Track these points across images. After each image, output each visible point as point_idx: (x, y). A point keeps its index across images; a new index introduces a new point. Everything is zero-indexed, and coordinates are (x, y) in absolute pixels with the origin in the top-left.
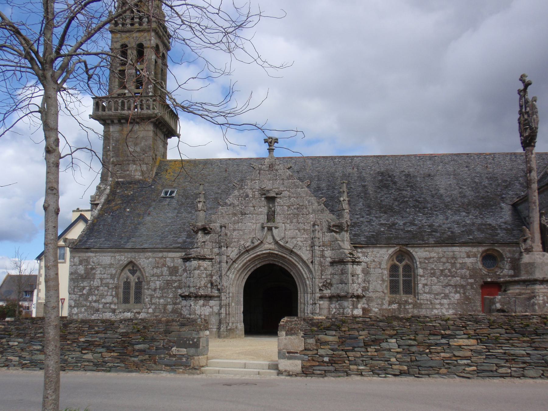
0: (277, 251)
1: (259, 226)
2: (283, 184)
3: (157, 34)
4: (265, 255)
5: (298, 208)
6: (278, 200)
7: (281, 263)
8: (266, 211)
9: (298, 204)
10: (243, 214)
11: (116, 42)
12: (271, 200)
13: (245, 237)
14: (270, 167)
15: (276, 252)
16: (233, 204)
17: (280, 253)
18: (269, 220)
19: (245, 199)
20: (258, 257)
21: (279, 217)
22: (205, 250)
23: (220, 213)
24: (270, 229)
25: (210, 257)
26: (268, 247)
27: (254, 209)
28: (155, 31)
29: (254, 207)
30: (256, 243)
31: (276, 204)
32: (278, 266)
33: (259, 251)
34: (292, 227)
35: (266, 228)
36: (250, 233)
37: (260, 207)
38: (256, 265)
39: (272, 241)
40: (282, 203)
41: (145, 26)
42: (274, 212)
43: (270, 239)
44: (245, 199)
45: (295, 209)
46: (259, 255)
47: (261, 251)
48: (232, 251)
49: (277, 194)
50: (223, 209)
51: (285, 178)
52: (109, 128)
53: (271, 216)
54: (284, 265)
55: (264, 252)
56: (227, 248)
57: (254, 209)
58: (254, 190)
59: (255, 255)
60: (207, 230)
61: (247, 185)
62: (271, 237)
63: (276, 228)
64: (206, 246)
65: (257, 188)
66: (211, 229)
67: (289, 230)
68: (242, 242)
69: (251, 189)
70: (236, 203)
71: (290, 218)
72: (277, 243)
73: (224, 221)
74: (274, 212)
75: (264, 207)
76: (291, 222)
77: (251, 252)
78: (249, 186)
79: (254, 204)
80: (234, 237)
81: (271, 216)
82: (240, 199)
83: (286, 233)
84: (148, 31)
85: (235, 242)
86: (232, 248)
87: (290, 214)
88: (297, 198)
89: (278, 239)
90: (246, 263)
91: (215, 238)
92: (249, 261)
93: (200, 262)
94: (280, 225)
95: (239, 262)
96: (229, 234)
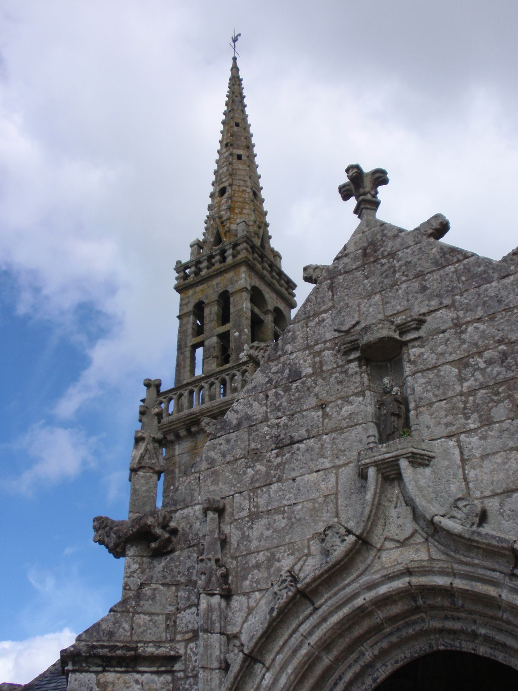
0: (442, 573)
1: (348, 473)
2: (424, 289)
3: (251, 268)
4: (395, 609)
5: (504, 356)
6: (414, 351)
7: (487, 639)
8: (371, 410)
9: (501, 342)
10: (284, 444)
11: (186, 304)
12: (381, 356)
13: (297, 538)
14: (365, 254)
15: (441, 581)
16: (248, 417)
17: (459, 584)
18: (385, 436)
19: (287, 389)
20: (366, 624)
21: (426, 418)
22: (141, 619)
23: (204, 466)
24: (390, 473)
25: (162, 651)
26: (400, 556)
27: (325, 415)
28: (246, 263)
29: (322, 406)
30: (340, 549)
31: (408, 369)
32: (475, 657)
33: (360, 588)
34: (493, 443)
35: (372, 472)
36: (314, 512)
37: (346, 400)
38: (369, 666)
39: (409, 527)
40: (431, 359)
41: (230, 260)
42: (406, 403)
43: (398, 522)
44: (287, 389)
45: (490, 362)
46: (362, 613)
47: (370, 587)
48: (250, 611)
49: (403, 329)
50: (214, 448)
51: (427, 266)
52: (174, 450)
53: (394, 418)
54: (504, 646)
55: (383, 590)
56: (227, 596)
57: (325, 415)
58: (317, 348)
59: (346, 610)
60: (155, 538)
61: (294, 338)
62: (404, 510)
63: (420, 460)
64: (146, 605)
65: (328, 336)
66: (174, 532)
67: (484, 457)
68: (286, 563)
69: (308, 347)
70: (258, 410)
71: (476, 408)
72: (434, 530)
73: (217, 490)
74: (403, 402)
75: (362, 393)
76: (488, 422)
77: (326, 601)
78: (300, 341)
79: (323, 395)
80: (254, 544)
81: (394, 418)
82: (271, 393)
83: (471, 474)
84: (235, 266)
85: (257, 566)
86: (247, 595)
87: (472, 392)
88: (492, 318)
89: (432, 509)
90: (311, 662)
91: (189, 564)
92: (326, 645)
93: (110, 676)
94: (437, 447)
95: (276, 656)
96: (235, 537)
